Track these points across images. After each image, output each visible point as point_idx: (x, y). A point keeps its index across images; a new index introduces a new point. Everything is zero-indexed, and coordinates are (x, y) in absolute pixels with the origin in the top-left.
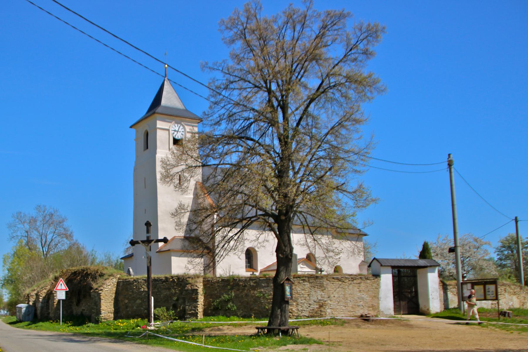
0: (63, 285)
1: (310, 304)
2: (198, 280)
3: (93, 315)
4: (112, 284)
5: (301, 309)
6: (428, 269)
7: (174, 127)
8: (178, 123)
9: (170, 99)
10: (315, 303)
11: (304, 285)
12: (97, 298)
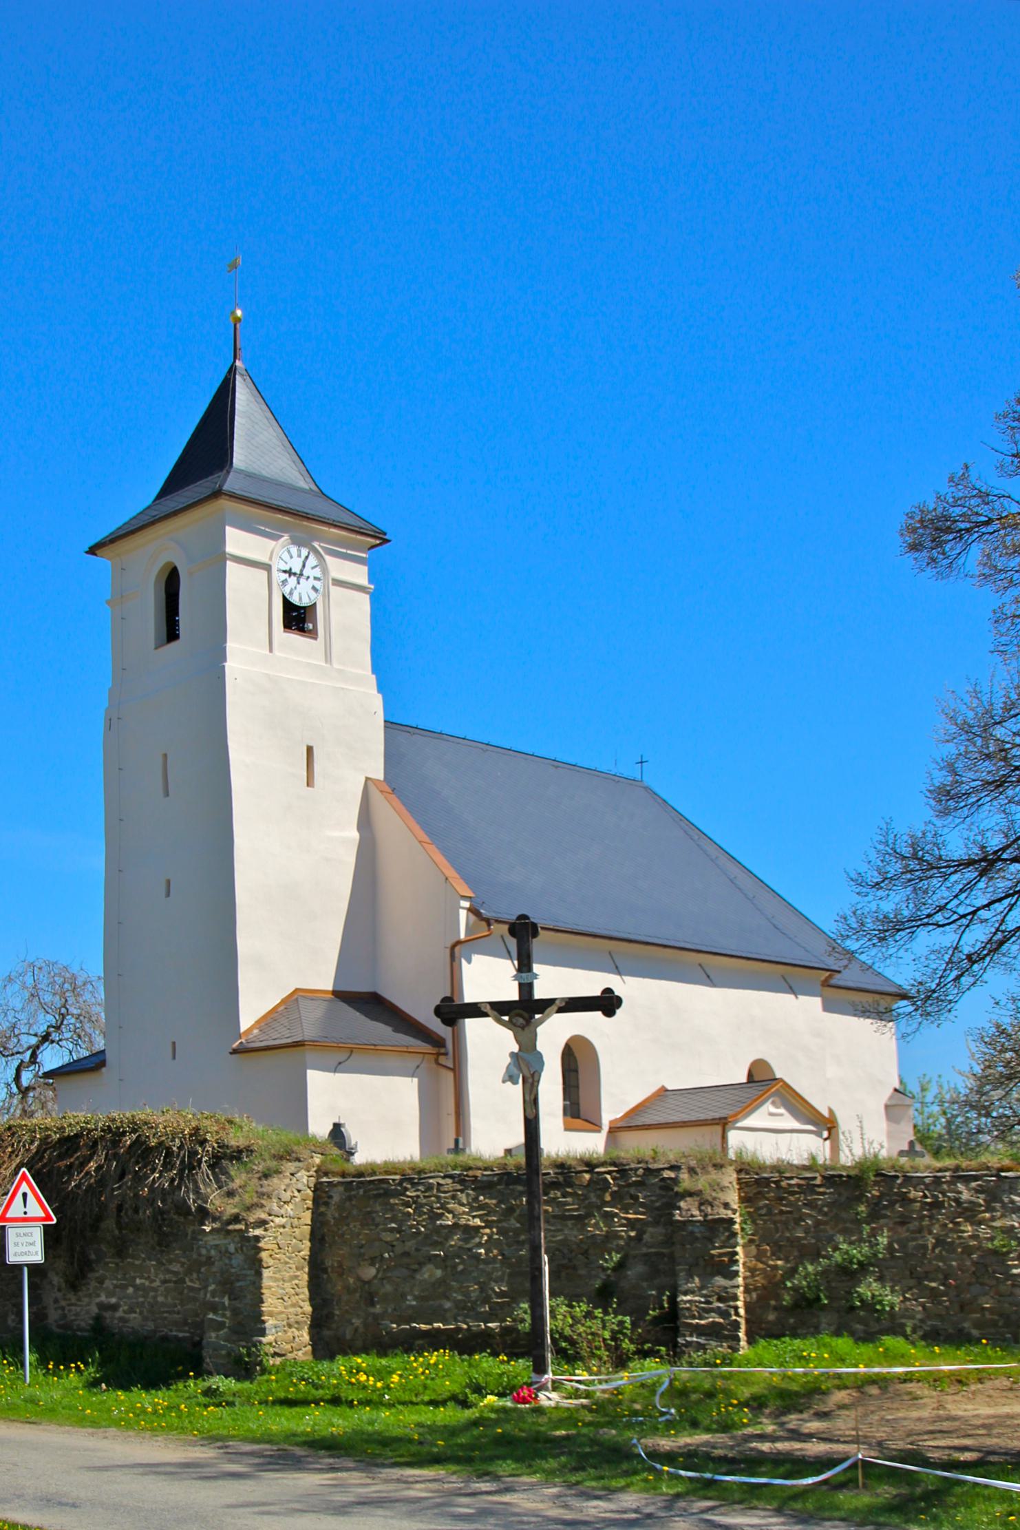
0: (30, 1196)
7: (286, 556)
8: (298, 542)
9: (256, 444)
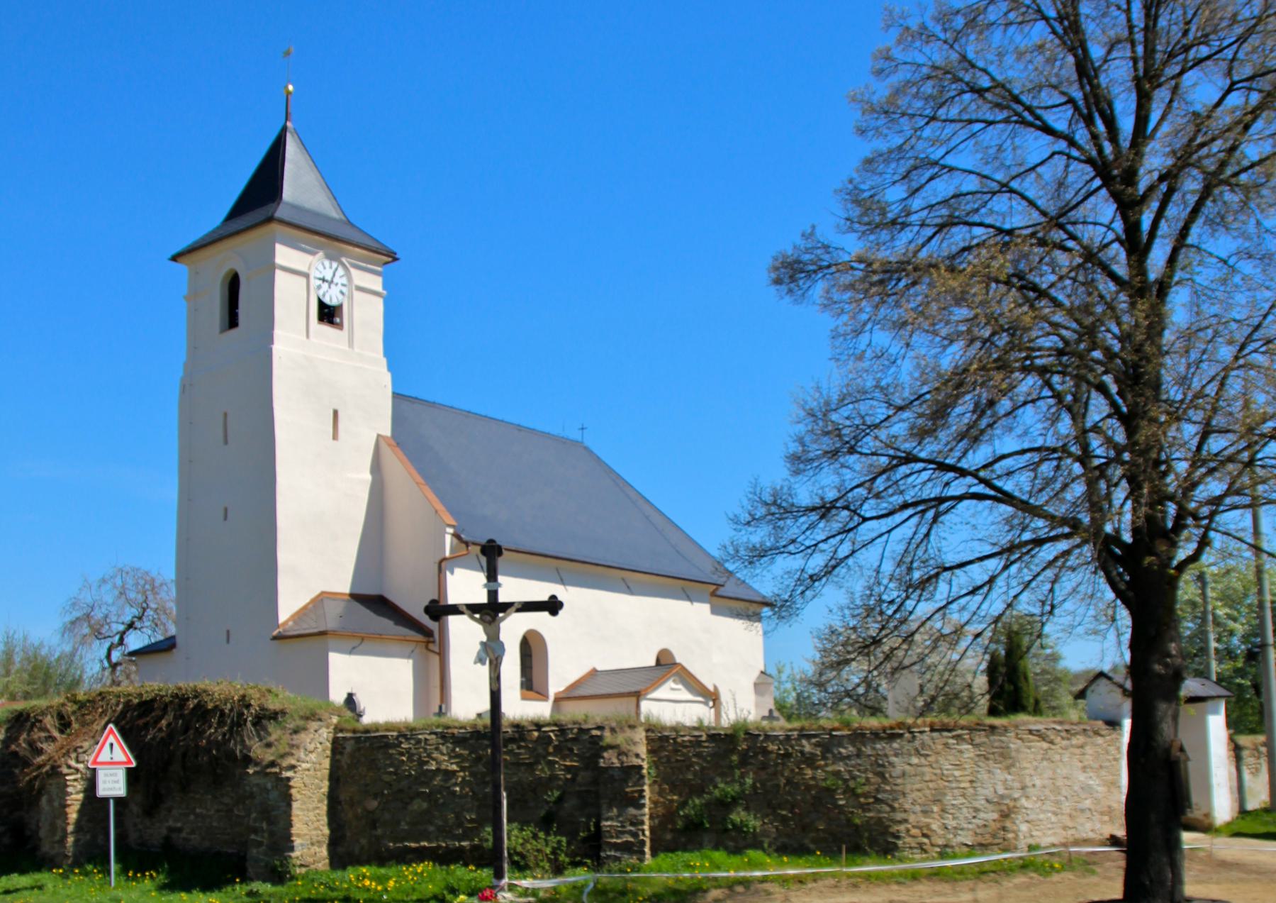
0: (116, 746)
1: (977, 810)
4: (320, 748)
5: (954, 823)
7: (321, 267)
8: (330, 257)
9: (300, 185)
10: (990, 807)
11: (961, 752)
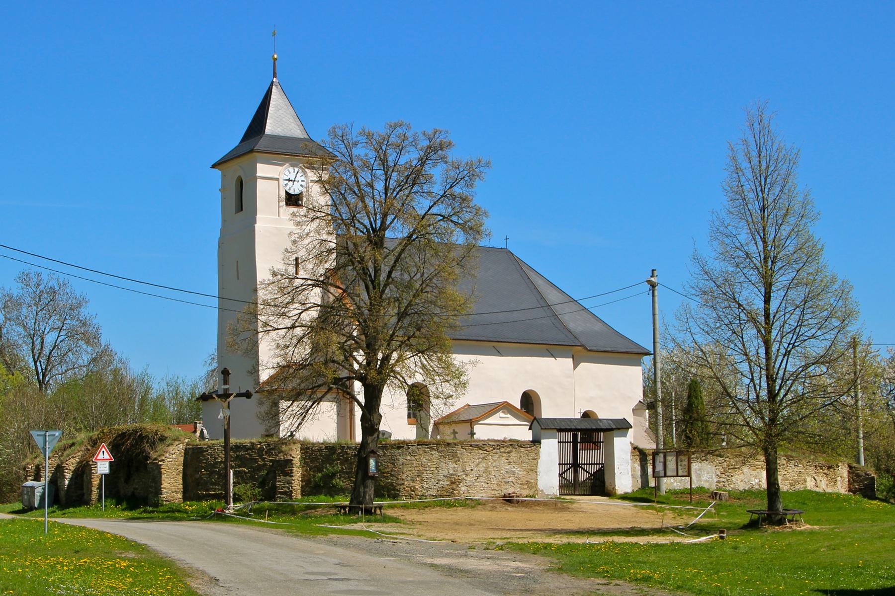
1: (439, 480)
2: (294, 447)
3: (150, 496)
6: (615, 432)
7: (287, 173)
8: (293, 166)
9: (281, 121)
12: (156, 472)
